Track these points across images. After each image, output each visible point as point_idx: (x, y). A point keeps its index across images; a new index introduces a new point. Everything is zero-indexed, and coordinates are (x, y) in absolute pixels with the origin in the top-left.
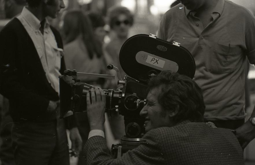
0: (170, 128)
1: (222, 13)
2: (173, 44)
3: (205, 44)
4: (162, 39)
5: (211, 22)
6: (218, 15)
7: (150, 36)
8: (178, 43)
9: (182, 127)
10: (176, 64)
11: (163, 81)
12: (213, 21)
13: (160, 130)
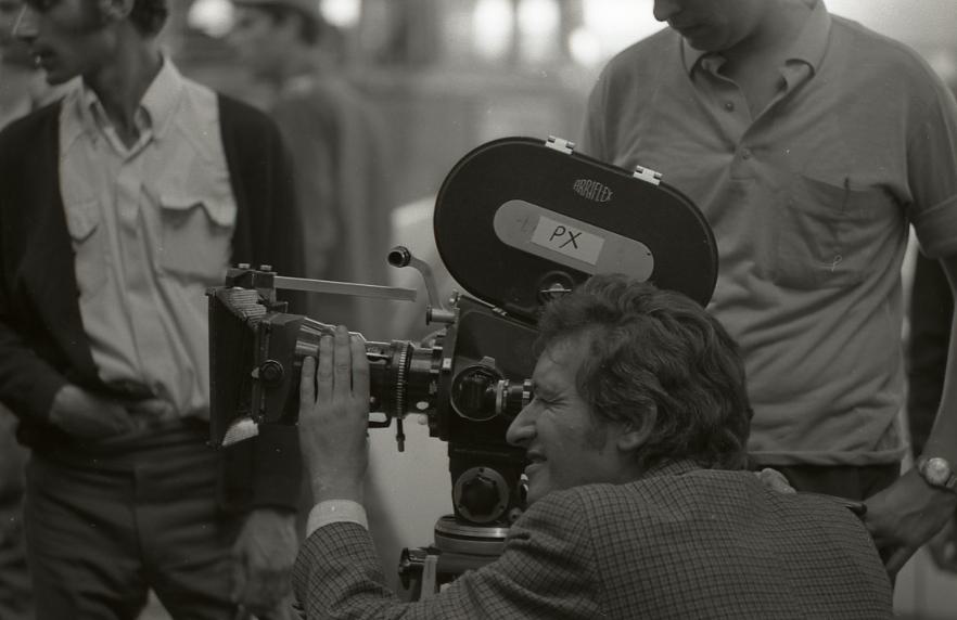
0: (621, 487)
3: (756, 177)
5: (780, 97)
6: (805, 69)
8: (565, 142)
10: (650, 261)
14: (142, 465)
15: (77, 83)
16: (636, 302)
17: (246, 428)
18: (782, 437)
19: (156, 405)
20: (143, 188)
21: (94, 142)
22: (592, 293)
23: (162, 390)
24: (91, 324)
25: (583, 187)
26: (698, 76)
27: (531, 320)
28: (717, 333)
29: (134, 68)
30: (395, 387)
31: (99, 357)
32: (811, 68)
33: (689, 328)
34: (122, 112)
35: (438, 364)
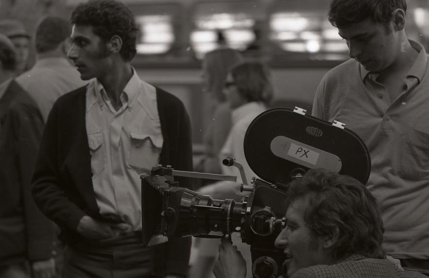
0: (331, 266)
1: (423, 78)
2: (295, 111)
3: (392, 129)
4: (320, 118)
5: (404, 92)
6: (415, 80)
7: (334, 124)
9: (352, 265)
11: (312, 187)
12: (406, 90)
13: (314, 269)
14: (117, 252)
15: (95, 79)
16: (329, 181)
17: (162, 239)
18: (403, 246)
19: (124, 225)
20: (123, 129)
21: (101, 106)
22: (310, 177)
23: (126, 219)
24: (97, 188)
25: (310, 130)
26: (367, 82)
27: (285, 189)
28: (366, 193)
29: (120, 75)
30: (226, 220)
31: (100, 204)
32: (418, 79)
33: (353, 192)
34: (115, 94)
35: (244, 210)
